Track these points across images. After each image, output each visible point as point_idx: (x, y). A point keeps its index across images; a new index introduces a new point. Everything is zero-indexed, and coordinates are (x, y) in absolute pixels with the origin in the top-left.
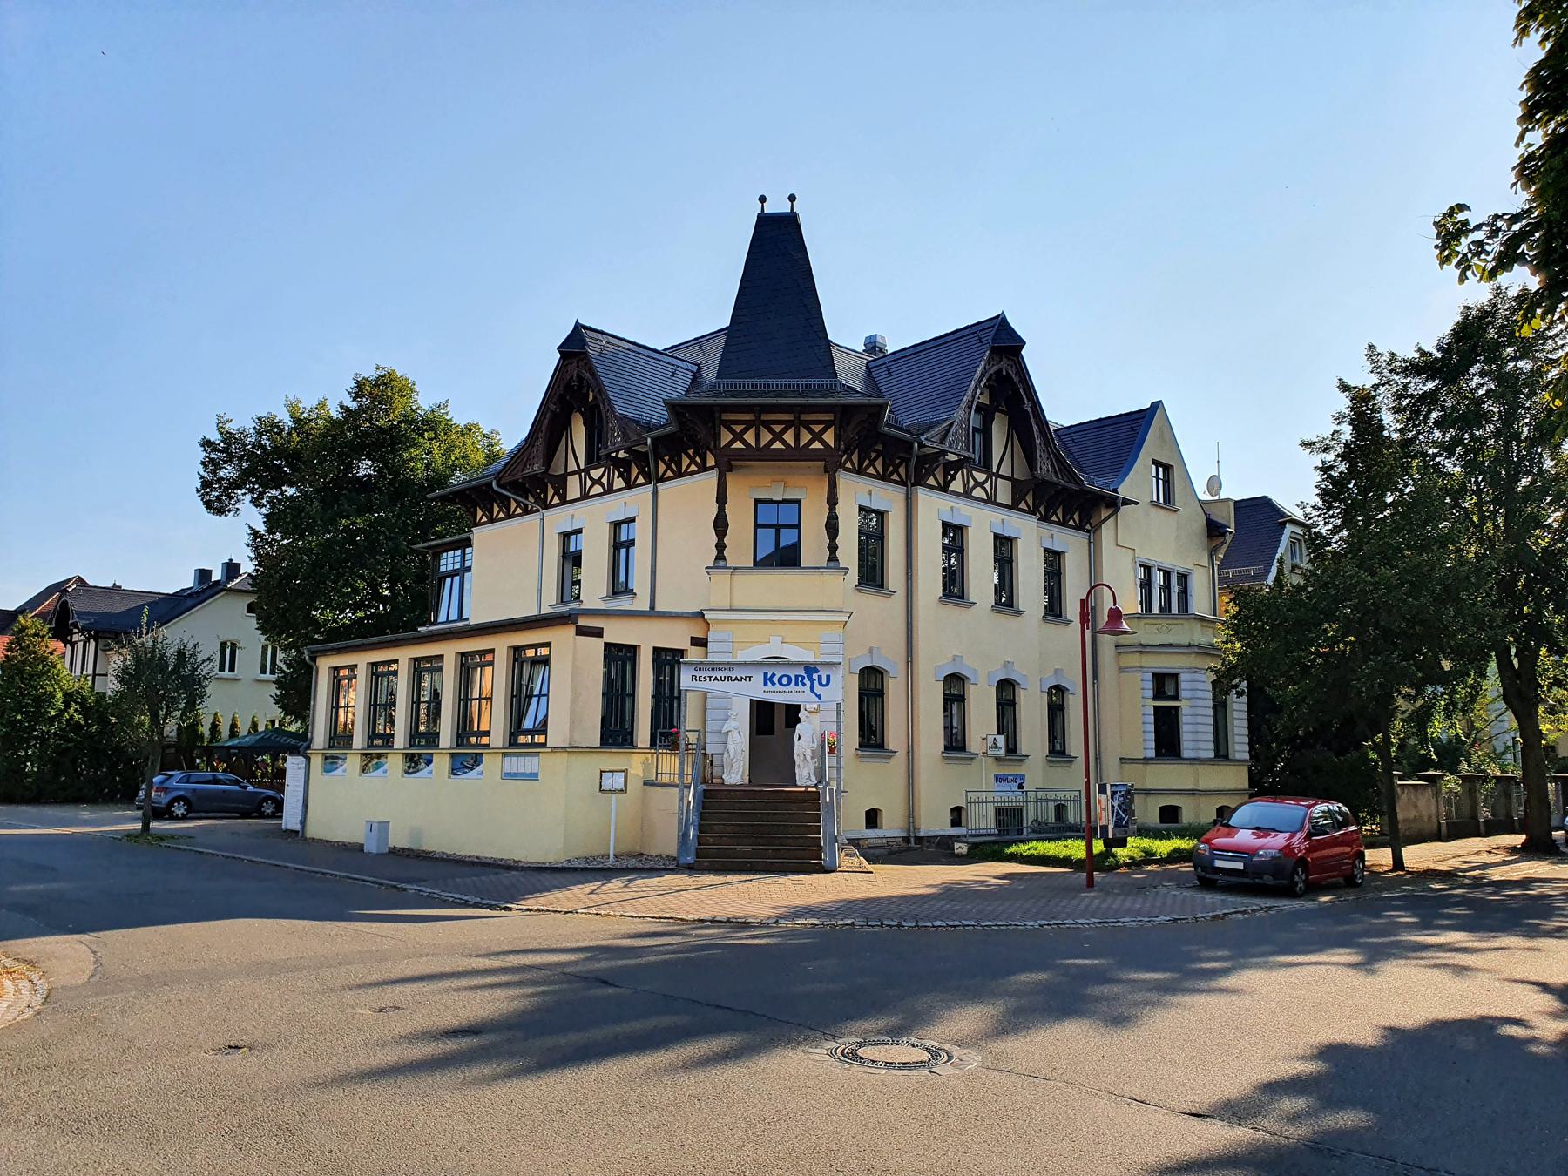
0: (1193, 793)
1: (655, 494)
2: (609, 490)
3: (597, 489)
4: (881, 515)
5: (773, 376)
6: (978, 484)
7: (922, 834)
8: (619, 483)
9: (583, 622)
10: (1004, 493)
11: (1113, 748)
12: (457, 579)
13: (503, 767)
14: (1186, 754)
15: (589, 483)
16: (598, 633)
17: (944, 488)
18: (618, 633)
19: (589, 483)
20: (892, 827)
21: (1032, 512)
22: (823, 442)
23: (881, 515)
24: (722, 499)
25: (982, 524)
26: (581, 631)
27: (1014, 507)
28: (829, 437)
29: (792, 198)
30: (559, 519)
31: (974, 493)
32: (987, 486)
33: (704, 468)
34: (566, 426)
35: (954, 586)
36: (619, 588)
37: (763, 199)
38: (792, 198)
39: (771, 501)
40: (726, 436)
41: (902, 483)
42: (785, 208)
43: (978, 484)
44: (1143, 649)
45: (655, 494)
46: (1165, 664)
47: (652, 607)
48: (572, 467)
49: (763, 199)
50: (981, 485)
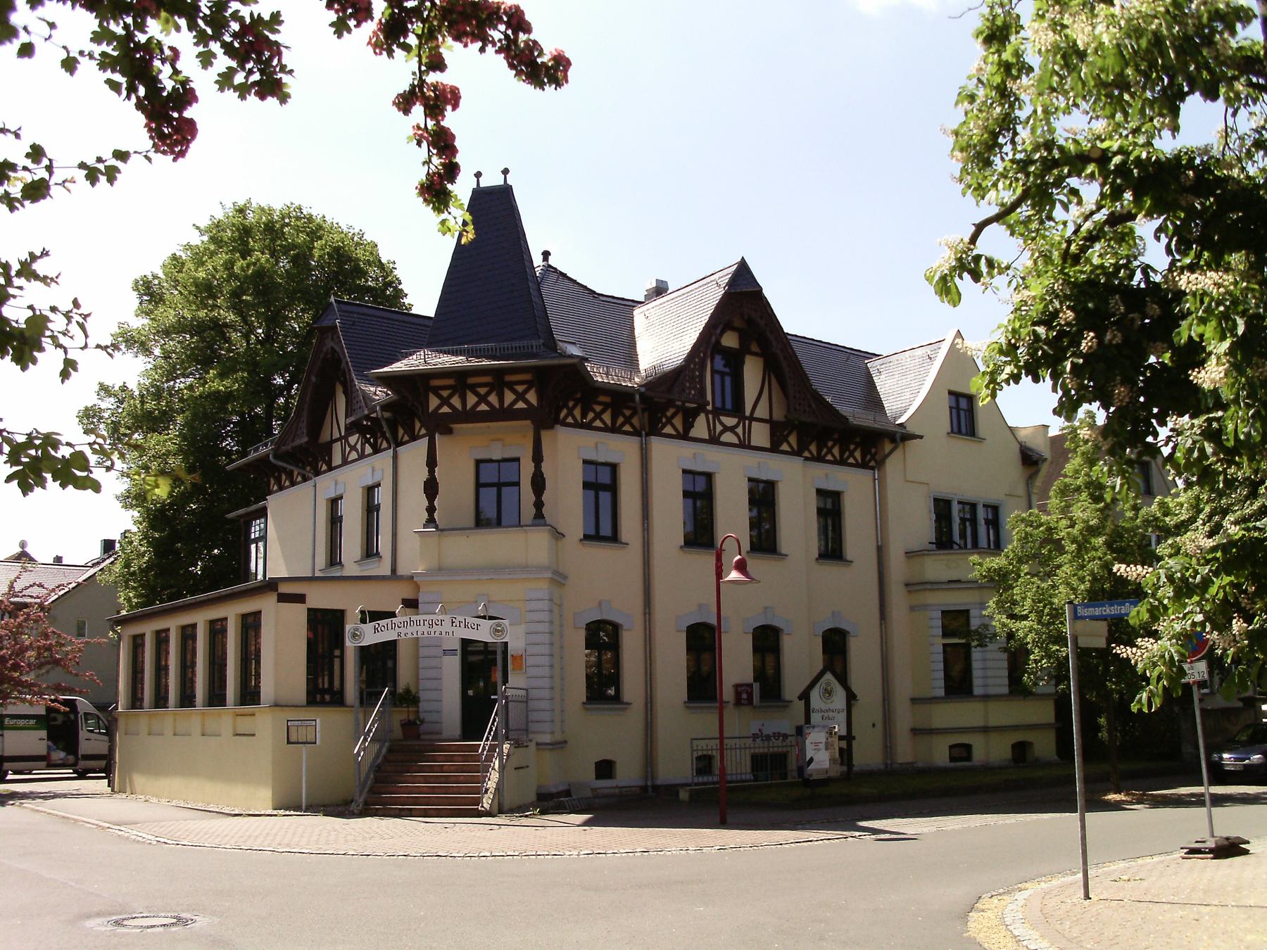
0: (985, 730)
1: (395, 457)
2: (362, 456)
3: (354, 455)
4: (614, 468)
5: (478, 342)
6: (726, 429)
7: (659, 782)
8: (368, 450)
9: (284, 589)
10: (760, 435)
11: (904, 688)
12: (261, 544)
13: (234, 728)
14: (977, 691)
15: (348, 449)
16: (300, 599)
17: (684, 436)
18: (321, 598)
19: (348, 449)
20: (628, 774)
21: (798, 453)
22: (526, 402)
23: (614, 468)
24: (432, 463)
25: (733, 472)
26: (284, 598)
27: (774, 448)
28: (532, 397)
29: (505, 172)
30: (326, 485)
31: (723, 439)
32: (739, 430)
33: (414, 438)
34: (332, 396)
35: (701, 534)
36: (370, 552)
37: (478, 175)
38: (505, 172)
39: (491, 461)
40: (434, 402)
41: (636, 433)
42: (498, 181)
43: (726, 429)
44: (934, 585)
45: (395, 457)
46: (955, 600)
47: (394, 570)
48: (336, 435)
49: (478, 175)
50: (732, 429)
